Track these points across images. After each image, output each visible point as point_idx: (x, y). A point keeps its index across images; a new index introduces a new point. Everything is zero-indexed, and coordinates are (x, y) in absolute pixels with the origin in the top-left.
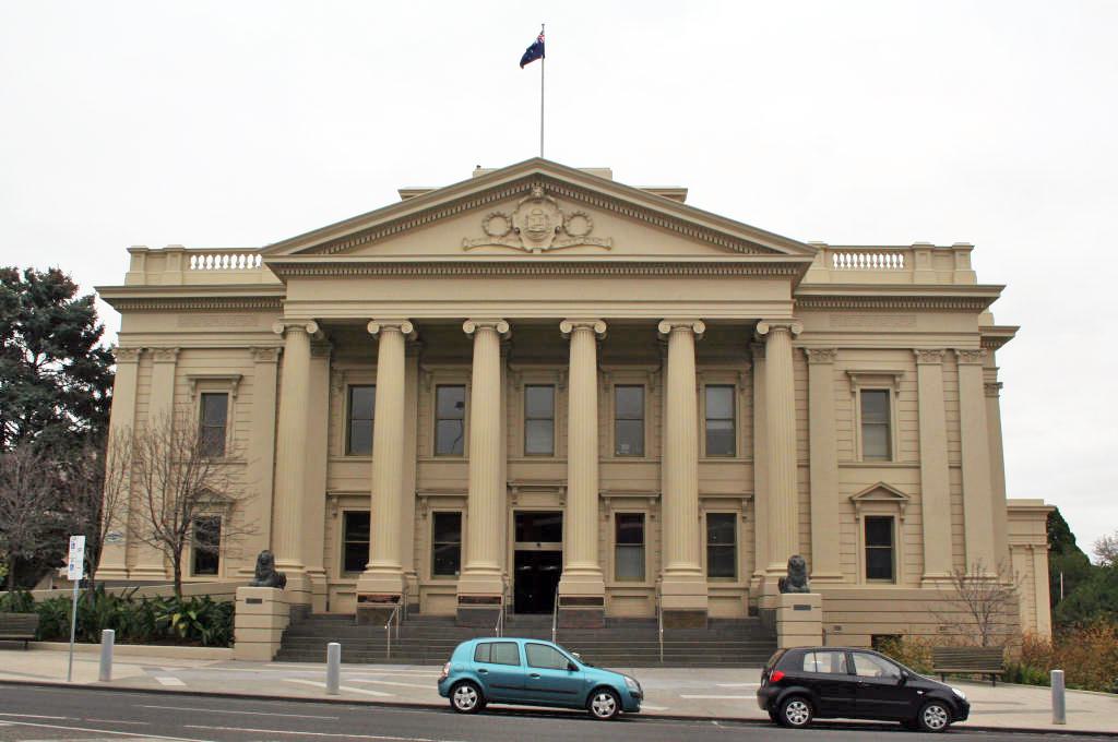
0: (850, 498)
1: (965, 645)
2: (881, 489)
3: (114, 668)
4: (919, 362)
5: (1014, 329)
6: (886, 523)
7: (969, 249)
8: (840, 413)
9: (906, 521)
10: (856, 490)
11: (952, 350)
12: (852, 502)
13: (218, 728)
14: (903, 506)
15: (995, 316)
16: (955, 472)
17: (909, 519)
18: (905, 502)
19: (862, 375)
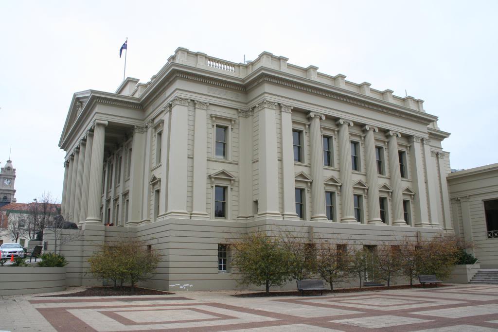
0: (209, 176)
1: (346, 261)
2: (223, 173)
3: (270, 289)
4: (196, 107)
5: (449, 134)
6: (225, 188)
7: (422, 102)
8: (431, 161)
9: (233, 190)
10: (212, 172)
11: (193, 101)
12: (210, 177)
13: (490, 322)
14: (232, 182)
15: (129, 77)
16: (190, 160)
17: (235, 189)
18: (234, 180)
19: (218, 118)
